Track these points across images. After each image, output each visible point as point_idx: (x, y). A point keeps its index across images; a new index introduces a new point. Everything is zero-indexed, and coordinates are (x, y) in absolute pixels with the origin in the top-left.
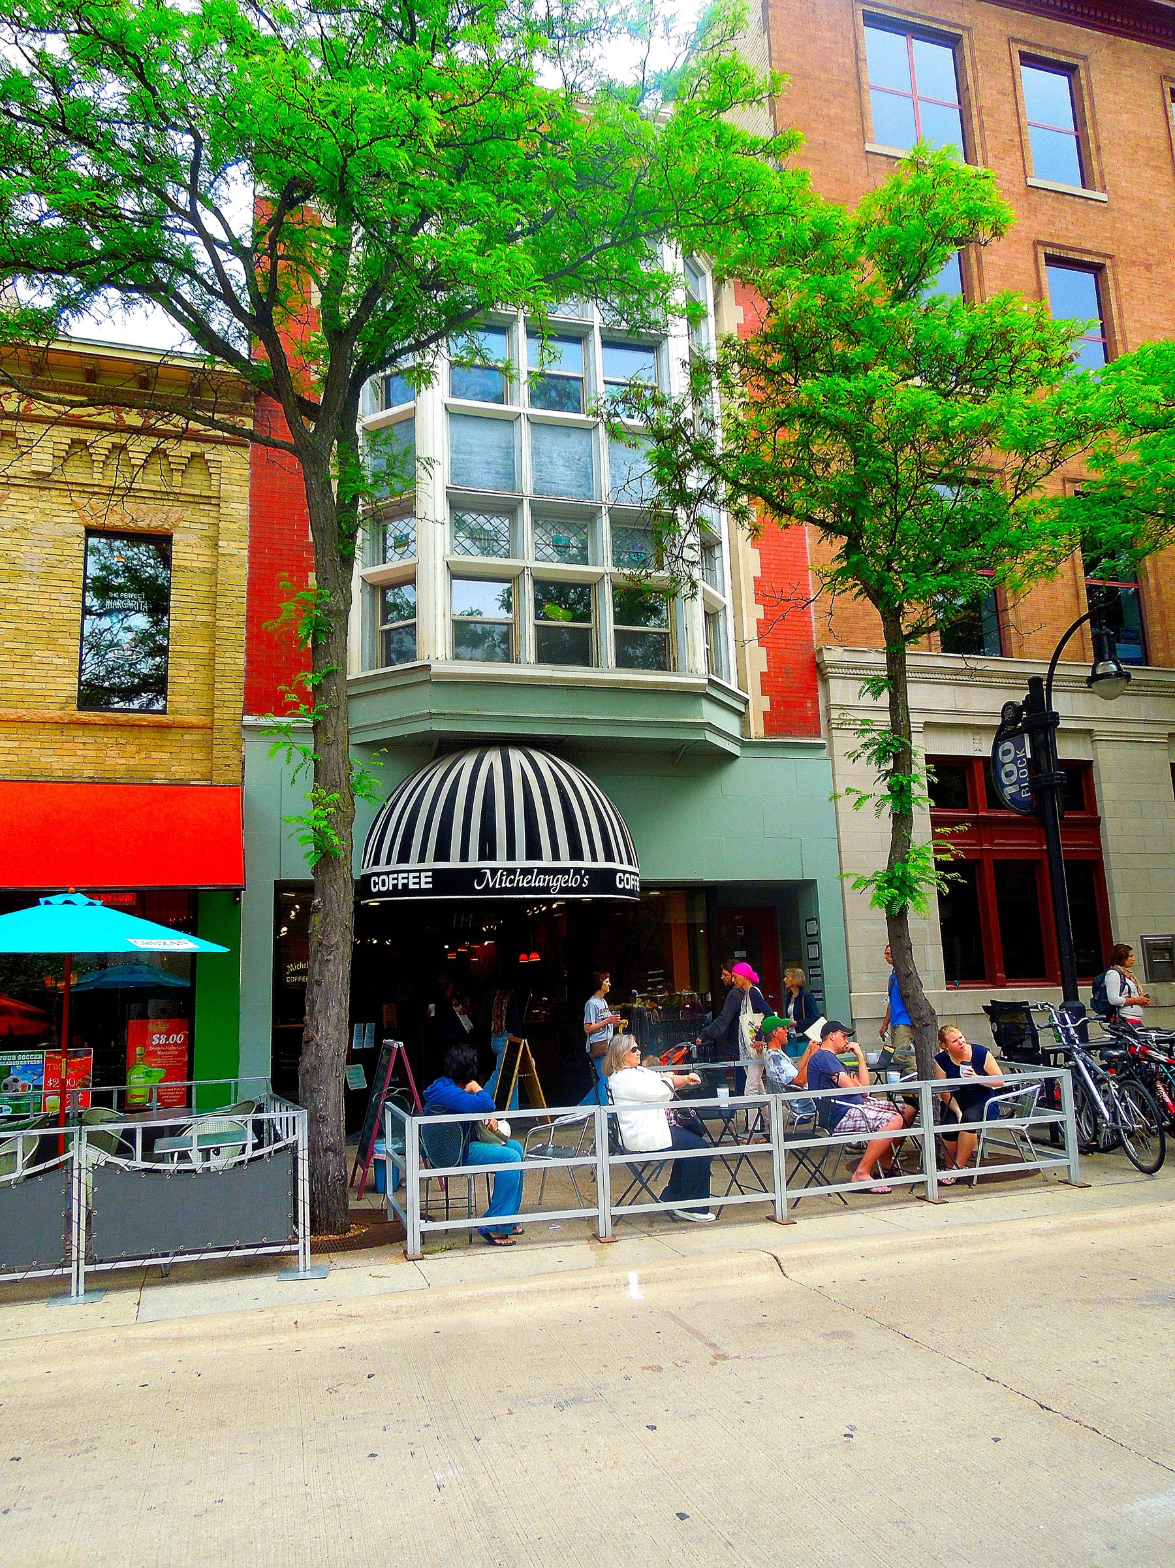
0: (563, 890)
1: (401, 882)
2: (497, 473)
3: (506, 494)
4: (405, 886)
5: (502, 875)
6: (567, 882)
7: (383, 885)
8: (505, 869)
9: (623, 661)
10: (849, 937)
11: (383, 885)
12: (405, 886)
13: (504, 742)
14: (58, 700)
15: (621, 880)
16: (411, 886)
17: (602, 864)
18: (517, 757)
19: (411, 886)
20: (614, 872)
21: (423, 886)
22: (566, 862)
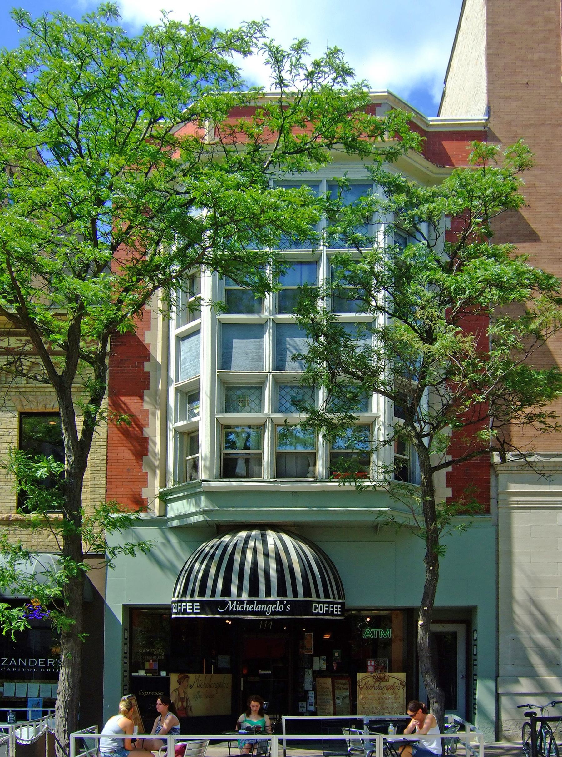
0: (273, 613)
1: (183, 607)
2: (253, 359)
3: (256, 372)
4: (332, 611)
5: (237, 604)
6: (253, 608)
7: (321, 610)
8: (237, 601)
9: (331, 474)
10: (500, 641)
11: (321, 610)
12: (332, 611)
13: (263, 527)
14: (7, 508)
15: (316, 608)
16: (188, 611)
17: (301, 598)
18: (271, 537)
19: (188, 611)
20: (311, 602)
21: (195, 611)
22: (323, 599)
